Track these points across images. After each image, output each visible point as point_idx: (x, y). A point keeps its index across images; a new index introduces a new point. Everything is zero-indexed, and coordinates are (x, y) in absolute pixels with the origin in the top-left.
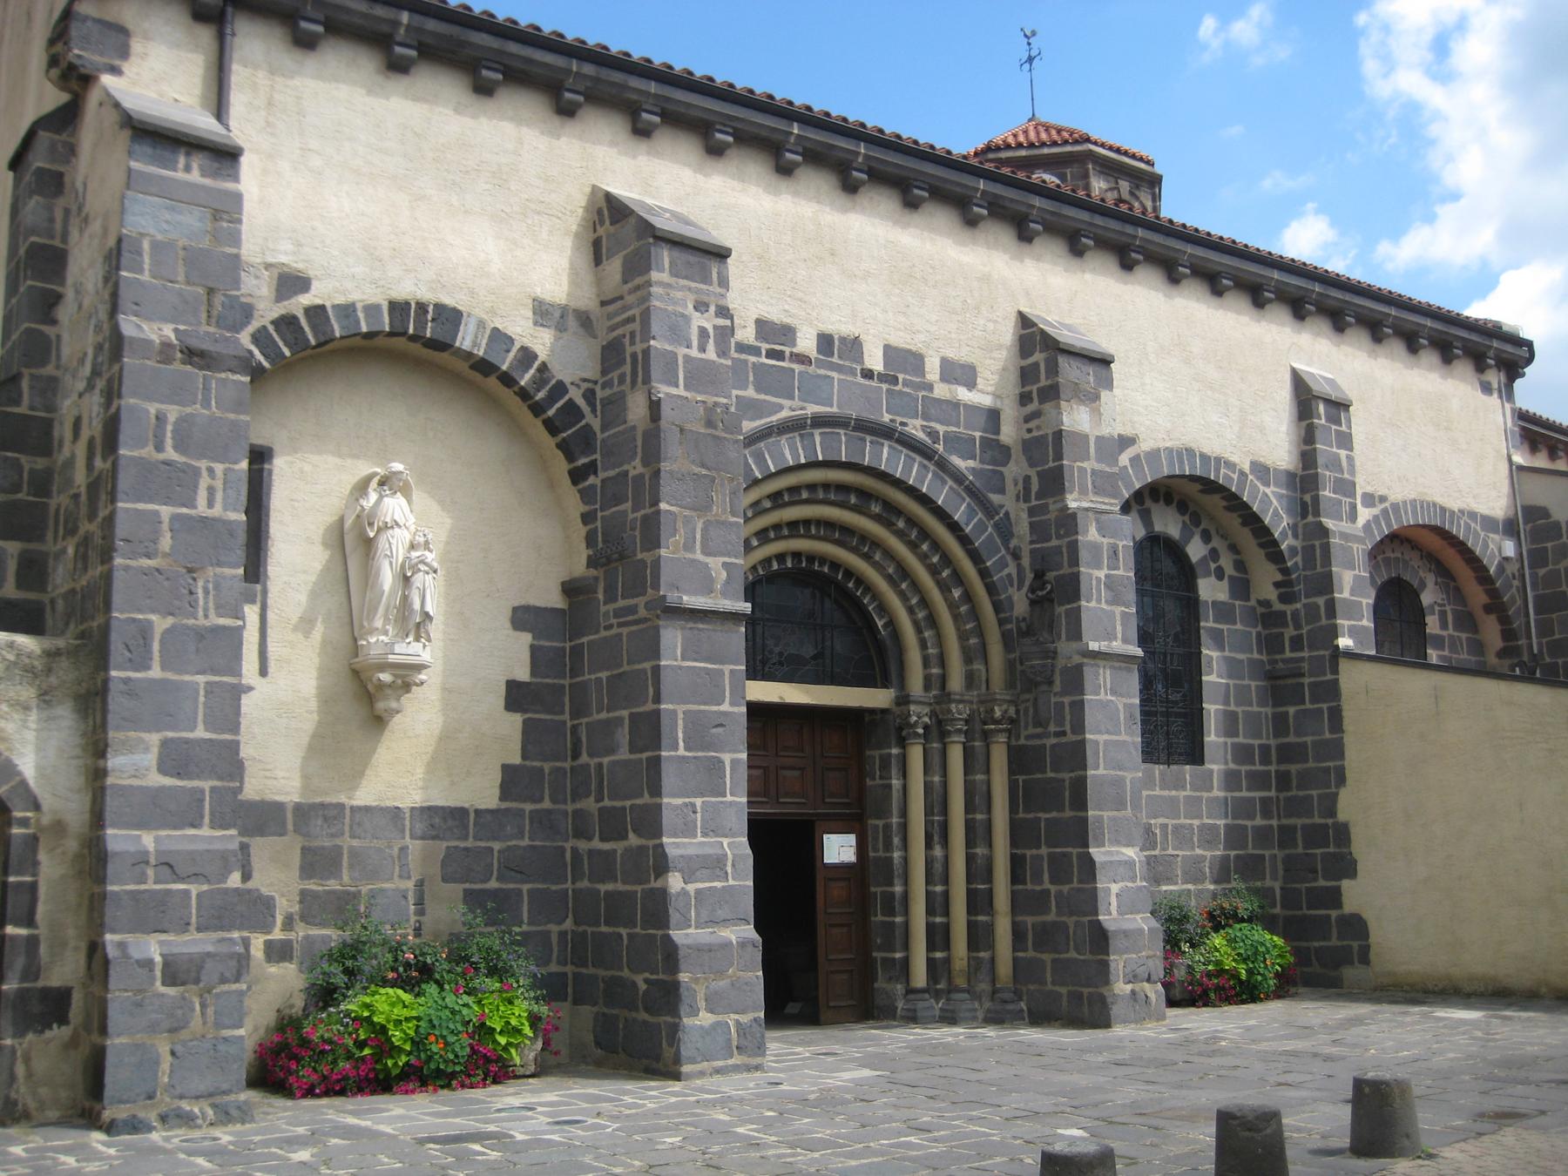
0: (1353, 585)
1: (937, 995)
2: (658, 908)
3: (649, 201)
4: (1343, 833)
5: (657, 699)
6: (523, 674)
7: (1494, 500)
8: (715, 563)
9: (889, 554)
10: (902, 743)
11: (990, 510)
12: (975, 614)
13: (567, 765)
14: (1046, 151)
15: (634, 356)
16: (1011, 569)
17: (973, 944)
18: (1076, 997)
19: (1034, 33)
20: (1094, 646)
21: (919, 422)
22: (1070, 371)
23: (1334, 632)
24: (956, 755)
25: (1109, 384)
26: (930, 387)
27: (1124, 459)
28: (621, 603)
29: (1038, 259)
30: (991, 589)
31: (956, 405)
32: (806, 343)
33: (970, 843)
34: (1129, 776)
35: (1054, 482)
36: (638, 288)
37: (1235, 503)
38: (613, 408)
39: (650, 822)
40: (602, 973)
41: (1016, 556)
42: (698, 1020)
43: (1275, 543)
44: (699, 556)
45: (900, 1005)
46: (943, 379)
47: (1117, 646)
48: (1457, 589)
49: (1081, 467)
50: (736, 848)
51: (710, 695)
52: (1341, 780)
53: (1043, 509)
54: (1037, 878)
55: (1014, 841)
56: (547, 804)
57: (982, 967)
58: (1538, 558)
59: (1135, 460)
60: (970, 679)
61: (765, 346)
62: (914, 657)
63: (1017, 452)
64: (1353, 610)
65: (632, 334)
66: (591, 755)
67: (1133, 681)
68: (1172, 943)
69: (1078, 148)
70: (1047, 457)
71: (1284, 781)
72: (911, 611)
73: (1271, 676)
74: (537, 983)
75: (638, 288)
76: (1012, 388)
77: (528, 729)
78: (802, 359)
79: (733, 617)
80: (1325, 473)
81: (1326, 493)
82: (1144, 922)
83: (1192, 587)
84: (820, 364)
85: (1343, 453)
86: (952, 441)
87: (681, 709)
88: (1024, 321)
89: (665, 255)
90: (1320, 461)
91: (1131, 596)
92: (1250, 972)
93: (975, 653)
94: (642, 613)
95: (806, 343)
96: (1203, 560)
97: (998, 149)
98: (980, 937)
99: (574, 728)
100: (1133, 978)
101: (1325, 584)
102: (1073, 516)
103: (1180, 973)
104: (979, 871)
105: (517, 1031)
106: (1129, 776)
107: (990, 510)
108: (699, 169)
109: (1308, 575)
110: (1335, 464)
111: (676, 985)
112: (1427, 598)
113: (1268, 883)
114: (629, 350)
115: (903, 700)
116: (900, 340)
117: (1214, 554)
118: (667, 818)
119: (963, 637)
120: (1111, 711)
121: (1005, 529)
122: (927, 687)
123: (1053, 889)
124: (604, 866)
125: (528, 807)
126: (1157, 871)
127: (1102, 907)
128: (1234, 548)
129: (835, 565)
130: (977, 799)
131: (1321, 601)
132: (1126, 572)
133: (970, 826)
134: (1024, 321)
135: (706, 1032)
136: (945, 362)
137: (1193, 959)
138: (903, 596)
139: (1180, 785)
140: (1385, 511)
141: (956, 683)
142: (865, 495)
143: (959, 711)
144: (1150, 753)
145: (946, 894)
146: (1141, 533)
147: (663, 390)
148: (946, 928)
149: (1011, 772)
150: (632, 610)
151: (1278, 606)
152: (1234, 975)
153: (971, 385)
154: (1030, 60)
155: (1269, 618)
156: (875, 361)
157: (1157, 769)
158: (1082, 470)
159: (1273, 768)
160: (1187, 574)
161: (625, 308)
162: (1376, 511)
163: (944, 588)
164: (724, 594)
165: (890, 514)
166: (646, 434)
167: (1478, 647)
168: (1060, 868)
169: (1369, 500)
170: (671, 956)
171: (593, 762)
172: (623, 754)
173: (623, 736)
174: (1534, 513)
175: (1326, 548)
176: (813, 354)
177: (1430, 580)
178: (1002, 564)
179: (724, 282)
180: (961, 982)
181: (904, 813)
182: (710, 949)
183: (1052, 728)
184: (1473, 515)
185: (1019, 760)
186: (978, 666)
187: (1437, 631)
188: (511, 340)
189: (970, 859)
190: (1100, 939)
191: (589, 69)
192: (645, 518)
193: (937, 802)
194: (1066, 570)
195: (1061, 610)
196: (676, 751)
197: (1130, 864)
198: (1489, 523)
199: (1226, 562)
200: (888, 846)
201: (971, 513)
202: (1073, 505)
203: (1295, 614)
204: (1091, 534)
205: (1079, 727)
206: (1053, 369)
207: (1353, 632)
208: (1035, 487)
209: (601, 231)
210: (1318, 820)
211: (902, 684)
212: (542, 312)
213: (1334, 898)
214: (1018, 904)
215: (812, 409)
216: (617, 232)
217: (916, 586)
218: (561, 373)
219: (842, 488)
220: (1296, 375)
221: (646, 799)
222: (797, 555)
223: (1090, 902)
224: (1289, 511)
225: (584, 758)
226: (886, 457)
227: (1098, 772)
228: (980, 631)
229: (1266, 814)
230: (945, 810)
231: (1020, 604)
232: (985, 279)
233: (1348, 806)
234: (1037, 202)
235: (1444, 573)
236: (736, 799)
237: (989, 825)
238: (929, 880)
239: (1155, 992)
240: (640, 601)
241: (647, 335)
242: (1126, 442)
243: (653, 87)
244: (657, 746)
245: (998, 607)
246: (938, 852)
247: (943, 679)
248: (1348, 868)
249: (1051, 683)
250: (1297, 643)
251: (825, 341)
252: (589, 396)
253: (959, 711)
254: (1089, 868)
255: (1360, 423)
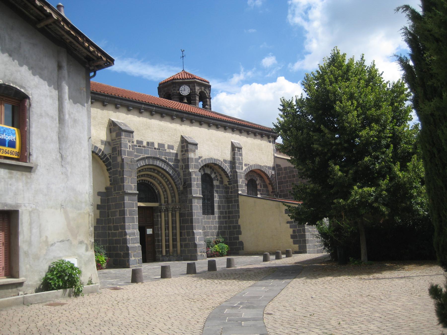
0: (242, 182)
1: (167, 256)
2: (125, 241)
3: (119, 121)
4: (239, 227)
5: (124, 207)
6: (99, 203)
7: (270, 163)
8: (133, 185)
9: (158, 179)
10: (160, 212)
11: (176, 171)
12: (173, 190)
13: (107, 218)
14: (186, 80)
15: (118, 150)
16: (180, 182)
17: (173, 247)
18: (192, 256)
19: (184, 51)
20: (194, 196)
21: (164, 157)
22: (190, 147)
23: (238, 191)
24: (170, 214)
25: (197, 149)
26: (166, 150)
27: (200, 161)
28: (117, 192)
29: (185, 125)
30: (176, 185)
31: (170, 153)
32: (145, 144)
33: (173, 230)
34: (200, 218)
35: (187, 167)
36: (119, 139)
37: (220, 167)
38: (115, 159)
39: (124, 228)
40: (114, 252)
41: (181, 179)
42: (132, 259)
43: (227, 174)
44: (130, 184)
45: (161, 258)
46: (168, 148)
47: (198, 195)
48: (264, 180)
49: (192, 164)
50: (137, 231)
51: (132, 205)
52: (239, 217)
53: (185, 171)
54: (184, 235)
55: (180, 229)
56: (104, 225)
57: (175, 251)
58: (279, 174)
59: (202, 161)
60: (172, 201)
61: (138, 145)
62: (162, 197)
63: (181, 161)
64: (242, 186)
65: (118, 147)
66: (111, 217)
67: (201, 201)
68: (208, 247)
69: (193, 80)
70: (186, 162)
71: (229, 217)
72: (162, 189)
73: (227, 198)
74: (106, 254)
75: (119, 139)
76: (180, 149)
77: (100, 212)
78: (144, 147)
79: (136, 194)
80: (237, 161)
81: (237, 165)
82: (203, 242)
83: (212, 183)
84: (147, 147)
85: (240, 157)
86: (170, 159)
87: (128, 209)
88: (182, 137)
89: (123, 134)
90: (236, 159)
91: (201, 186)
92: (222, 251)
93: (173, 196)
94: (121, 193)
95: (145, 144)
96: (214, 177)
97: (176, 79)
98: (175, 246)
99: (108, 212)
100: (201, 252)
101: (236, 182)
102: (191, 173)
103: (210, 252)
104: (174, 235)
105: (103, 261)
106: (200, 218)
107: (176, 171)
108: (127, 114)
109: (234, 179)
110: (239, 159)
111: (129, 253)
112: (257, 182)
113: (226, 236)
114: (117, 149)
115: (161, 205)
116: (160, 142)
117: (216, 176)
118: (126, 227)
119: (171, 194)
120: (197, 206)
121: (179, 175)
122: (165, 203)
123: (187, 237)
124: (114, 235)
125: (101, 225)
126: (205, 234)
127: (196, 240)
128: (220, 175)
129: (149, 181)
130: (174, 222)
131: (236, 185)
132: (200, 182)
133: (172, 227)
134: (182, 137)
135: (133, 260)
136: (168, 145)
137: (212, 249)
138: (161, 187)
139: (210, 219)
140: (249, 167)
141: (170, 201)
142: (154, 170)
143: (170, 207)
144: (204, 213)
145: (169, 239)
146: (203, 173)
147: (124, 157)
148: (169, 245)
149: (180, 217)
150: (119, 193)
151: (228, 186)
152: (219, 252)
153: (173, 149)
154: (183, 57)
155: (227, 188)
156: (156, 146)
157: (206, 216)
158: (192, 164)
159: (227, 215)
160: (211, 180)
161: (117, 142)
162: (247, 167)
163: (168, 185)
164: (134, 190)
165: (159, 172)
166: (121, 164)
167: (268, 191)
168: (188, 234)
169: (246, 165)
170: (128, 248)
171: (112, 218)
172: (118, 216)
173: (118, 213)
174: (278, 166)
175: (237, 175)
176: (146, 146)
177: (258, 178)
178: (178, 181)
179: (133, 137)
180: (171, 254)
181: (161, 225)
182: (134, 247)
183: (187, 210)
184: (266, 166)
185: (181, 215)
186: (174, 199)
187: (260, 188)
188: (97, 147)
189: (173, 233)
190: (195, 246)
191: (109, 98)
192: (121, 178)
193: (167, 223)
194: (189, 182)
195: (188, 189)
196: (127, 216)
197: (201, 233)
198: (269, 168)
199: (219, 178)
200: (158, 231)
201: (173, 172)
202: (190, 171)
203: (231, 187)
204: (194, 176)
205: (192, 209)
206: (187, 147)
207: (241, 190)
208: (184, 167)
209: (111, 127)
210: (235, 224)
211: (160, 202)
212: (102, 142)
213: (238, 238)
214: (181, 240)
215: (146, 156)
216: (113, 127)
217: (163, 185)
218: (106, 153)
219: (151, 169)
220: (232, 142)
221: (122, 224)
222: (142, 180)
223: (193, 239)
224: (230, 168)
225: (110, 217)
226: (158, 163)
227: (195, 217)
228: (174, 193)
229: (226, 224)
230: (168, 224)
231: (181, 188)
232: (175, 130)
233: (240, 222)
234: (185, 115)
235: (261, 177)
236: (137, 223)
237: (176, 226)
238: (165, 236)
239: (205, 254)
240: (121, 192)
241: (121, 147)
242: (200, 157)
243: (119, 101)
244: (125, 215)
245: (177, 188)
246: (167, 231)
247: (168, 201)
248: (240, 233)
249: (186, 202)
250: (231, 192)
251: (148, 143)
252: (110, 156)
253: (170, 207)
254: (193, 233)
255: (244, 151)
